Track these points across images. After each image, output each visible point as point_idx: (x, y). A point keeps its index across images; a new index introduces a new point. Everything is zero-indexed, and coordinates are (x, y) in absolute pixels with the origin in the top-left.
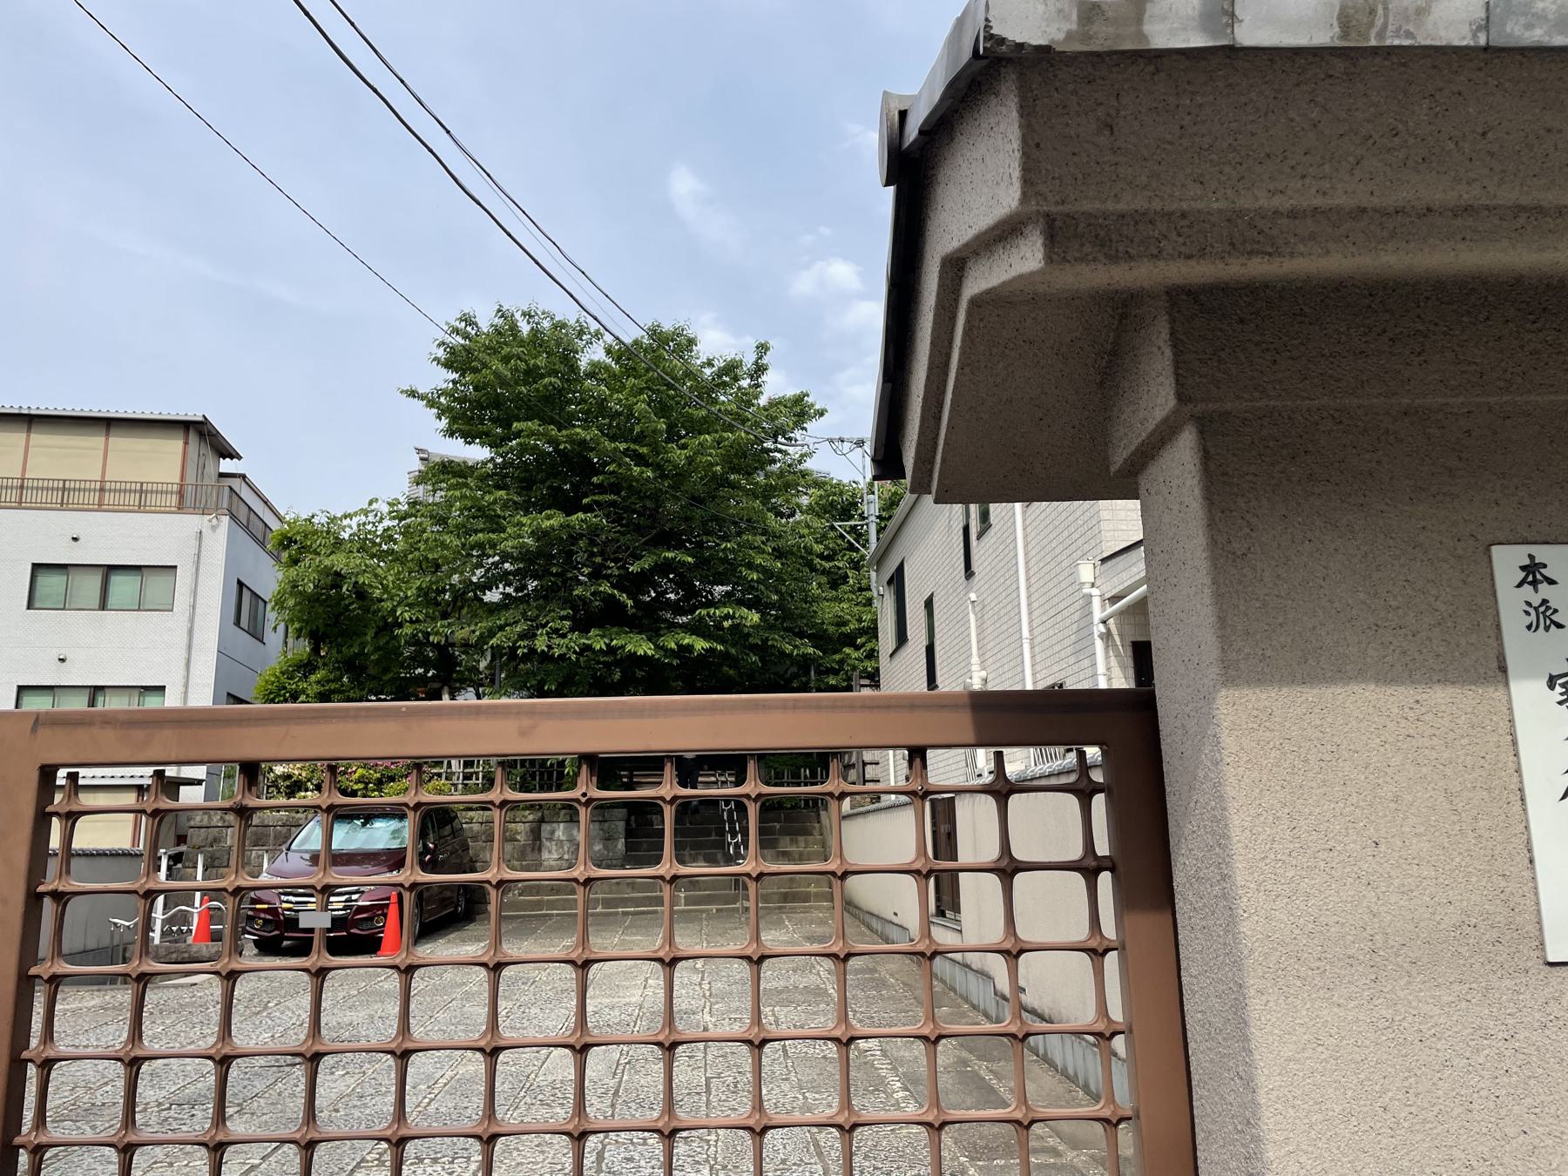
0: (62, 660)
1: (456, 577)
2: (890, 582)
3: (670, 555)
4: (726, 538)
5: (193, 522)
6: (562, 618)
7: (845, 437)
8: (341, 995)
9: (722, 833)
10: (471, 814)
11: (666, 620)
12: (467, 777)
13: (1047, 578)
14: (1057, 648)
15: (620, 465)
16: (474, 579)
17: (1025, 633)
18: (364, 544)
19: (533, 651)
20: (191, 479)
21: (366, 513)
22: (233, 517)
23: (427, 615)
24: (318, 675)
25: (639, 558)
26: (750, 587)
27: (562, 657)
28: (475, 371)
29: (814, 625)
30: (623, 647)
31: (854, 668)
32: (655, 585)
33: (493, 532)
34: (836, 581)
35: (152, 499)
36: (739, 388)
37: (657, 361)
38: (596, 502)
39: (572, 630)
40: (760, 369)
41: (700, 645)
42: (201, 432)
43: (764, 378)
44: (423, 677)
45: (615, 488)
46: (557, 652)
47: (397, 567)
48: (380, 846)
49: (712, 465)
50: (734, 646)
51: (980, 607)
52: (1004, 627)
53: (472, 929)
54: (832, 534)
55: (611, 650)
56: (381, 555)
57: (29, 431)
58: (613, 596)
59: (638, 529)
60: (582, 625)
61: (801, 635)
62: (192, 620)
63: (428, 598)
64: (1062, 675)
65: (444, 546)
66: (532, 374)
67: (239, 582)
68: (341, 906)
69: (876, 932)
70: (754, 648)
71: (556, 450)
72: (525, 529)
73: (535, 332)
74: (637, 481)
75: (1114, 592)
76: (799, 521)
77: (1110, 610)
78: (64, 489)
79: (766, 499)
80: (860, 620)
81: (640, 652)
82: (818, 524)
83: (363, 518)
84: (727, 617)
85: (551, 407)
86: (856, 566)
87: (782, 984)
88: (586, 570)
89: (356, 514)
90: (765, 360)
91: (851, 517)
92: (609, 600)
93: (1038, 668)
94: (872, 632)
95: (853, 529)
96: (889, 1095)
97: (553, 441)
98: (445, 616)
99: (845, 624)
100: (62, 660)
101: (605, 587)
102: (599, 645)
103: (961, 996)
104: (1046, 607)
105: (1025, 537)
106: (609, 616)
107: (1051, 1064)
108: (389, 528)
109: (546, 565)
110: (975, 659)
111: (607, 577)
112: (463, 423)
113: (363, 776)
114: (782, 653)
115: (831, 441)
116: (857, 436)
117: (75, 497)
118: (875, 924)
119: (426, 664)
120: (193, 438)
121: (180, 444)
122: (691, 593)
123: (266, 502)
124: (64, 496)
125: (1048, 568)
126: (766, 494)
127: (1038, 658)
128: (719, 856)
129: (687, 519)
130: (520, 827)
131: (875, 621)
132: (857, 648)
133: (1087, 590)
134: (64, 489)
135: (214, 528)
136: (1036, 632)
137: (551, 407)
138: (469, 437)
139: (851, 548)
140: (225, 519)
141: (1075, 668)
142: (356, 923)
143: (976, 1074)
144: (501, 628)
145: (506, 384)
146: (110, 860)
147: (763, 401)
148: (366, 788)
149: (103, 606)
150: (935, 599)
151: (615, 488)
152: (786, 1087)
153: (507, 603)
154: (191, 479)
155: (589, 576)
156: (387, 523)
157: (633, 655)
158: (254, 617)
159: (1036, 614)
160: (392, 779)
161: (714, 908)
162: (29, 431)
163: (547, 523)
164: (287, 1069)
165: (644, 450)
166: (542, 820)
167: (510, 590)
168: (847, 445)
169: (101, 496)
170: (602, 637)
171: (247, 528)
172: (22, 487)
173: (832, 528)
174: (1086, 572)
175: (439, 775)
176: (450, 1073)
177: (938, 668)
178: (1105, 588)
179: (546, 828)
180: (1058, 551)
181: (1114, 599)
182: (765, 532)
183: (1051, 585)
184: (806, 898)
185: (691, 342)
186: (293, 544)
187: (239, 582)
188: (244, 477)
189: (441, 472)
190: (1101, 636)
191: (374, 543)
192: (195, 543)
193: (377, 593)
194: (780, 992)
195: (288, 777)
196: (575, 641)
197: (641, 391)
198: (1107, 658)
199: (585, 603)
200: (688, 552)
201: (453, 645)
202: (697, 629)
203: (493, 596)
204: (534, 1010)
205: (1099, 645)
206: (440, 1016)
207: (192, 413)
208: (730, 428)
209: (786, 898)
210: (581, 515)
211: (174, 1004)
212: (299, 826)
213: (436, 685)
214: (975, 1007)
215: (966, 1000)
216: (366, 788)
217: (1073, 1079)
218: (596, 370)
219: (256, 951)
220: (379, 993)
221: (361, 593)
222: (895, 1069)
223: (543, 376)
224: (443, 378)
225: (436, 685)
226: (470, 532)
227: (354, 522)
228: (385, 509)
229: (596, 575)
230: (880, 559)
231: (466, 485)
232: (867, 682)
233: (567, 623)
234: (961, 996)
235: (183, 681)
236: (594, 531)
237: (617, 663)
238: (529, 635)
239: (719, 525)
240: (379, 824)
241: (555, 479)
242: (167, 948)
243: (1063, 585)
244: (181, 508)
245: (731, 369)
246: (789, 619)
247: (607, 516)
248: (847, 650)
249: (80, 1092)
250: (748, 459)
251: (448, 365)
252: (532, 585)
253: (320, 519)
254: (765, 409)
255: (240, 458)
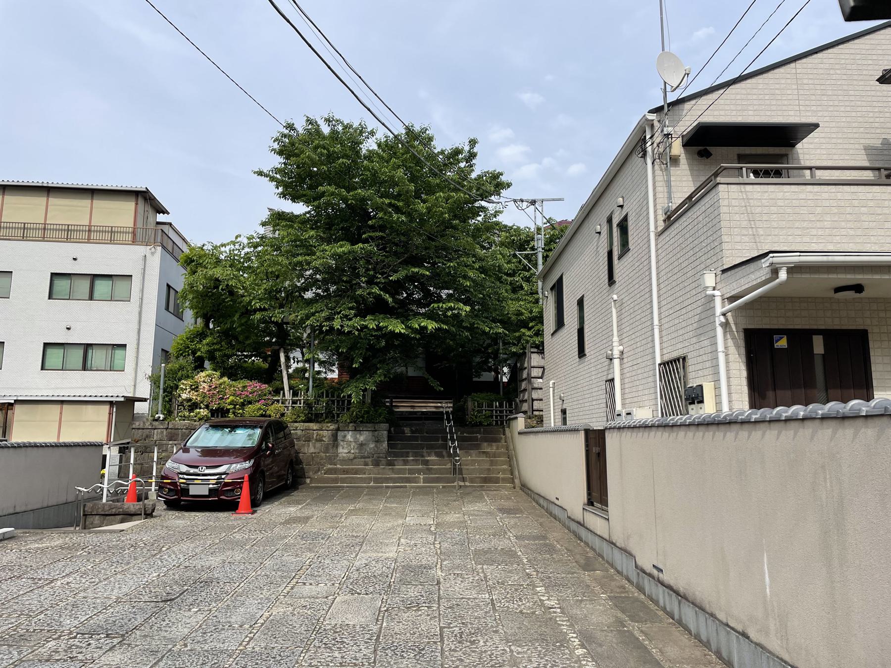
0: (69, 329)
1: (287, 283)
2: (552, 289)
3: (416, 270)
4: (450, 260)
5: (141, 250)
6: (350, 309)
7: (524, 198)
8: (209, 542)
9: (445, 439)
10: (296, 424)
11: (413, 311)
12: (294, 402)
13: (674, 284)
14: (681, 332)
15: (385, 214)
16: (299, 284)
17: (656, 322)
18: (232, 262)
19: (332, 328)
20: (140, 225)
21: (234, 243)
22: (164, 247)
23: (271, 305)
24: (208, 340)
25: (396, 272)
26: (465, 290)
27: (349, 332)
28: (297, 155)
29: (503, 315)
30: (386, 327)
31: (527, 342)
32: (406, 289)
33: (308, 255)
34: (516, 289)
35: (117, 237)
36: (459, 168)
37: (411, 148)
38: (371, 237)
39: (356, 316)
40: (472, 155)
41: (431, 325)
42: (144, 197)
43: (474, 161)
44: (270, 342)
45: (382, 228)
46: (346, 330)
47: (253, 277)
48: (239, 445)
49: (442, 213)
50: (453, 326)
51: (620, 304)
52: (638, 317)
53: (296, 495)
54: (514, 260)
55: (379, 328)
56: (244, 270)
57: (48, 196)
58: (380, 295)
59: (396, 254)
60: (362, 314)
61: (494, 321)
62: (141, 306)
63: (271, 295)
64: (685, 351)
65: (280, 264)
66: (331, 157)
67: (168, 286)
68: (214, 482)
69: (543, 507)
70: (466, 328)
71: (347, 205)
72: (330, 253)
73: (334, 132)
74: (396, 223)
75: (733, 293)
76: (497, 254)
77: (728, 307)
78: (68, 230)
79: (474, 237)
80: (531, 312)
81: (397, 331)
82: (507, 252)
83: (232, 246)
84: (451, 309)
85: (342, 178)
86: (527, 280)
87: (486, 546)
88: (364, 279)
89: (228, 244)
90: (475, 150)
91: (525, 250)
92: (378, 298)
93: (665, 345)
94: (540, 319)
95: (527, 257)
96: (572, 652)
97: (345, 200)
98: (281, 306)
99: (522, 314)
100: (69, 329)
101: (376, 290)
102: (372, 325)
103: (608, 562)
104: (673, 304)
105: (657, 256)
106: (378, 308)
107: (687, 629)
108: (248, 253)
109: (340, 277)
110: (616, 339)
111: (377, 284)
112: (291, 191)
113: (233, 401)
114: (484, 332)
115: (515, 201)
116: (531, 197)
117: (75, 235)
118: (541, 501)
119: (271, 334)
120: (141, 201)
121: (133, 204)
122: (427, 294)
123: (184, 239)
124: (68, 234)
125: (675, 277)
126: (477, 232)
127: (665, 339)
128: (444, 453)
129: (426, 248)
130: (325, 433)
131: (541, 313)
132: (530, 329)
133: (710, 292)
134: (68, 230)
135: (153, 254)
136: (663, 321)
137: (342, 178)
138: (295, 199)
139: (525, 269)
140: (159, 249)
141: (696, 346)
142: (224, 493)
143: (631, 634)
144: (313, 314)
145: (316, 164)
146: (83, 449)
147: (474, 175)
148: (234, 408)
149: (91, 298)
150: (585, 299)
151: (382, 228)
152: (496, 639)
153: (317, 298)
154: (140, 225)
155: (367, 282)
156: (247, 250)
157: (392, 333)
158: (177, 306)
159: (664, 309)
160: (250, 403)
161: (441, 485)
162: (48, 196)
163: (341, 250)
164: (161, 604)
165: (401, 204)
166: (338, 429)
167: (319, 291)
168: (525, 204)
169: (89, 234)
170: (374, 320)
171: (172, 254)
172: (45, 229)
173: (515, 256)
174: (709, 279)
175: (278, 401)
176: (267, 614)
177: (586, 343)
178: (724, 290)
179: (340, 434)
180: (683, 265)
181: (732, 299)
182: (474, 256)
183: (677, 289)
184: (497, 481)
185: (430, 139)
186: (193, 261)
187: (168, 286)
188: (170, 224)
189: (278, 219)
190: (722, 325)
191: (240, 262)
192: (142, 262)
193: (241, 292)
194: (486, 552)
195: (190, 400)
196: (357, 322)
197: (399, 167)
198: (725, 340)
199: (364, 299)
200: (427, 269)
201: (287, 323)
202: (431, 316)
203: (309, 295)
204: (327, 561)
205: (720, 331)
206: (267, 563)
207: (140, 186)
208: (456, 190)
209: (486, 480)
210: (360, 245)
211: (104, 546)
212: (195, 430)
213: (277, 347)
214: (619, 572)
215: (612, 566)
216: (234, 408)
217: (707, 645)
218: (371, 155)
219: (165, 507)
220: (231, 542)
221: (231, 292)
222: (572, 625)
223: (339, 158)
224: (278, 161)
225: (277, 347)
226: (295, 255)
227: (227, 249)
228: (246, 241)
229: (371, 282)
230: (545, 276)
231: (292, 227)
232: (536, 350)
233: (353, 312)
234: (608, 562)
235: (136, 342)
236: (368, 256)
237: (384, 336)
238: (330, 319)
239: (448, 252)
240: (239, 431)
241: (347, 223)
242: (110, 505)
243: (688, 289)
244: (134, 242)
245: (457, 152)
246: (485, 308)
247: (377, 246)
248: (523, 330)
249: (23, 618)
250: (464, 211)
251: (280, 153)
252: (333, 288)
253: (208, 247)
254: (475, 179)
255: (168, 213)
